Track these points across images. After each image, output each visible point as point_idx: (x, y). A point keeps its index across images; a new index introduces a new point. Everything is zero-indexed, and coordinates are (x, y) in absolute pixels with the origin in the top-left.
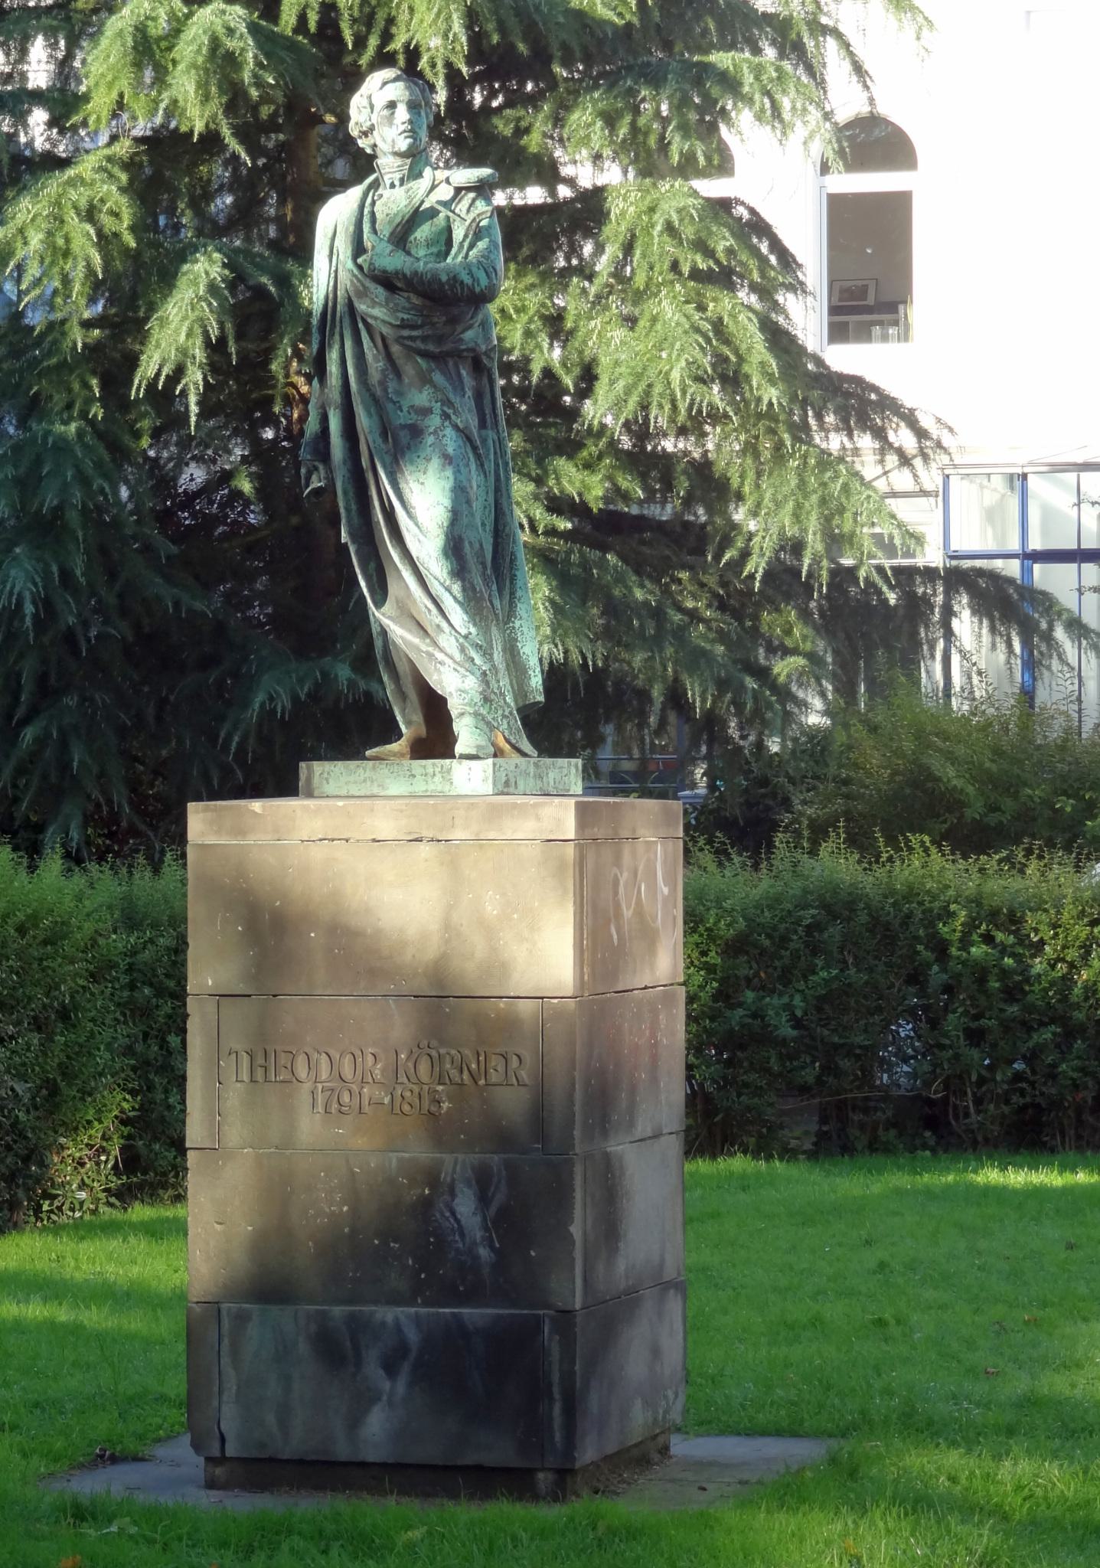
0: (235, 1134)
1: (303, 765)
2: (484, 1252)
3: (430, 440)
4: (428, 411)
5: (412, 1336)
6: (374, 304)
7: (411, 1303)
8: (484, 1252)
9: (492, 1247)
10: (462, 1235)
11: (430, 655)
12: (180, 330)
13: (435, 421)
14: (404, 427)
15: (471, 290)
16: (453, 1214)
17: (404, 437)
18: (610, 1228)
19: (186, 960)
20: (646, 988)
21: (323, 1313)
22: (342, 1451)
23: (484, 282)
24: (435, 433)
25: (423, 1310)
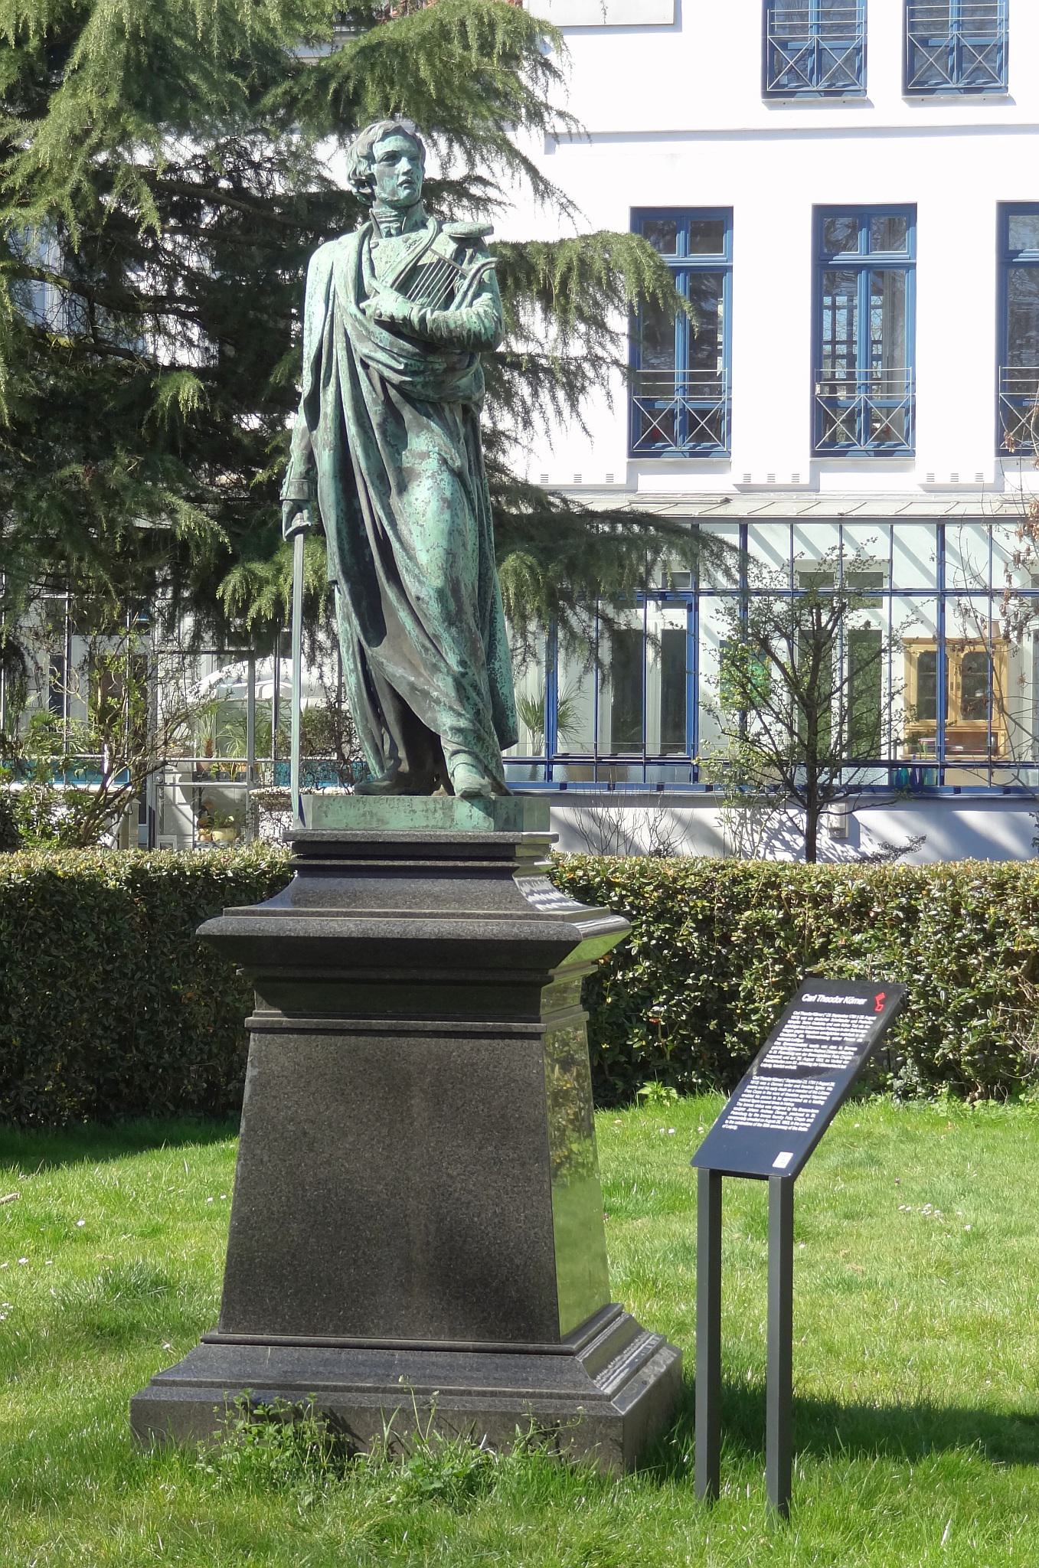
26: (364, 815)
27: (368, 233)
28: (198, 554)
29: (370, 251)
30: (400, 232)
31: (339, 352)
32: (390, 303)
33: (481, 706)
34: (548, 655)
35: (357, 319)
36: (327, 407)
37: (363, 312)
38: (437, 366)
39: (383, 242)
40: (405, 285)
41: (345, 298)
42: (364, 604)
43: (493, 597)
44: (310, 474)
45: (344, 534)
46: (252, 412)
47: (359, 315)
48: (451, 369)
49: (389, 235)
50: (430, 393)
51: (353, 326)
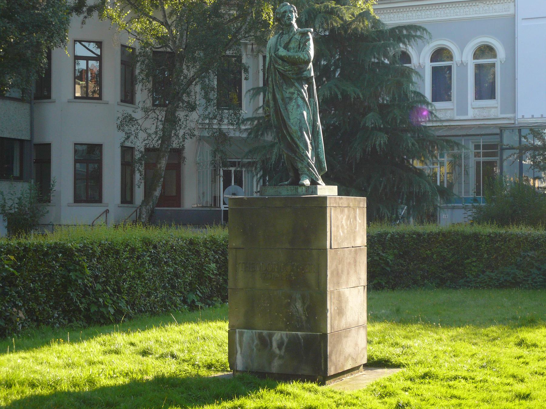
0: (241, 285)
1: (362, 202)
2: (303, 317)
3: (294, 101)
4: (294, 93)
5: (286, 340)
6: (279, 65)
7: (285, 331)
8: (303, 317)
9: (306, 316)
10: (298, 313)
11: (294, 158)
12: (385, 102)
13: (295, 96)
14: (287, 97)
15: (304, 60)
16: (296, 307)
17: (287, 100)
18: (340, 312)
19: (367, 258)
20: (129, 217)
21: (261, 333)
22: (267, 370)
23: (307, 58)
24: (295, 99)
25: (288, 332)
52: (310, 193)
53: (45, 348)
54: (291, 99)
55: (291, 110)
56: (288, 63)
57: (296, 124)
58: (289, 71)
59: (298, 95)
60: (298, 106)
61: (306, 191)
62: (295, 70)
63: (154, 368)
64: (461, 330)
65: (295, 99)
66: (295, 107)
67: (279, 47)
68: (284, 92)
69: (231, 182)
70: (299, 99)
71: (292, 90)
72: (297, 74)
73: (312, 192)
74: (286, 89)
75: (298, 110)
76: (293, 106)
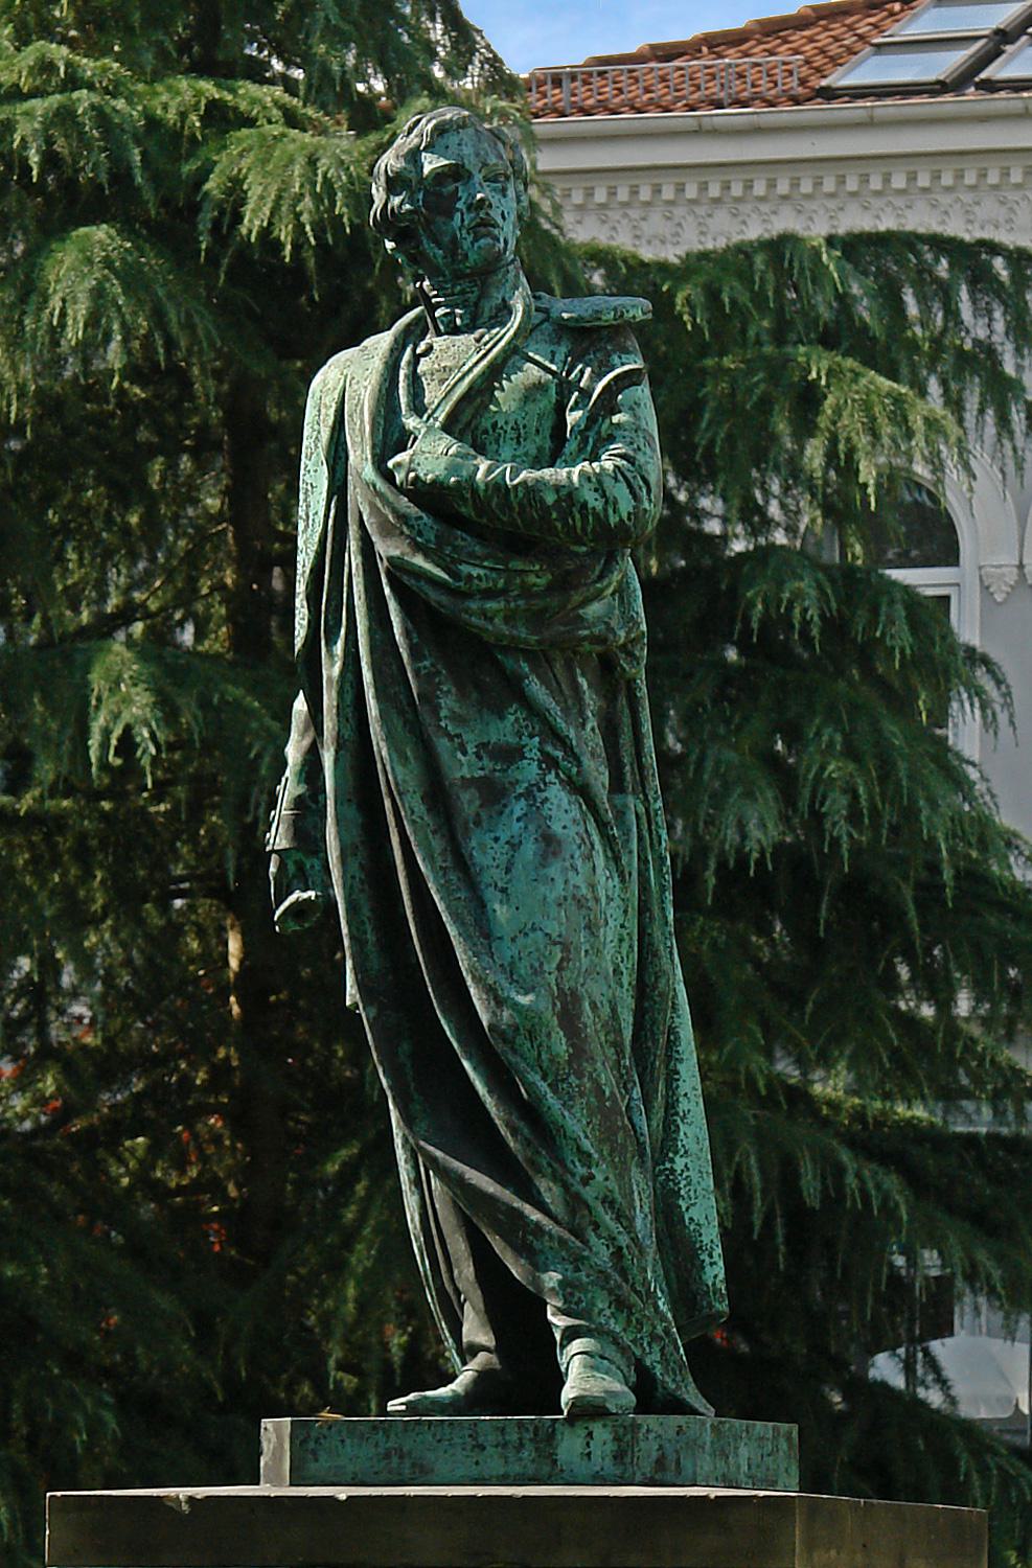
3: (519, 808)
13: (530, 770)
14: (467, 783)
17: (468, 803)
24: (529, 794)
26: (387, 1456)
27: (415, 332)
28: (568, 1102)
29: (416, 359)
30: (469, 328)
31: (354, 559)
32: (431, 454)
33: (624, 1240)
34: (495, 1053)
35: (378, 494)
36: (332, 670)
37: (388, 476)
38: (532, 579)
39: (440, 343)
40: (469, 420)
41: (360, 459)
42: (405, 1047)
43: (672, 1031)
44: (308, 808)
45: (366, 912)
46: (923, 1019)
47: (381, 485)
48: (563, 584)
49: (455, 331)
50: (523, 633)
51: (372, 506)
52: (647, 1467)
53: (856, 230)
54: (493, 793)
55: (496, 875)
56: (480, 535)
57: (537, 971)
58: (489, 594)
59: (549, 762)
60: (550, 844)
61: (618, 1457)
62: (527, 592)
63: (340, 882)
64: (957, 1309)
65: (529, 794)
66: (529, 850)
67: (411, 422)
68: (443, 745)
69: (292, 905)
70: (557, 796)
71: (505, 728)
72: (537, 619)
73: (660, 1463)
74: (455, 718)
75: (554, 870)
76: (514, 846)
